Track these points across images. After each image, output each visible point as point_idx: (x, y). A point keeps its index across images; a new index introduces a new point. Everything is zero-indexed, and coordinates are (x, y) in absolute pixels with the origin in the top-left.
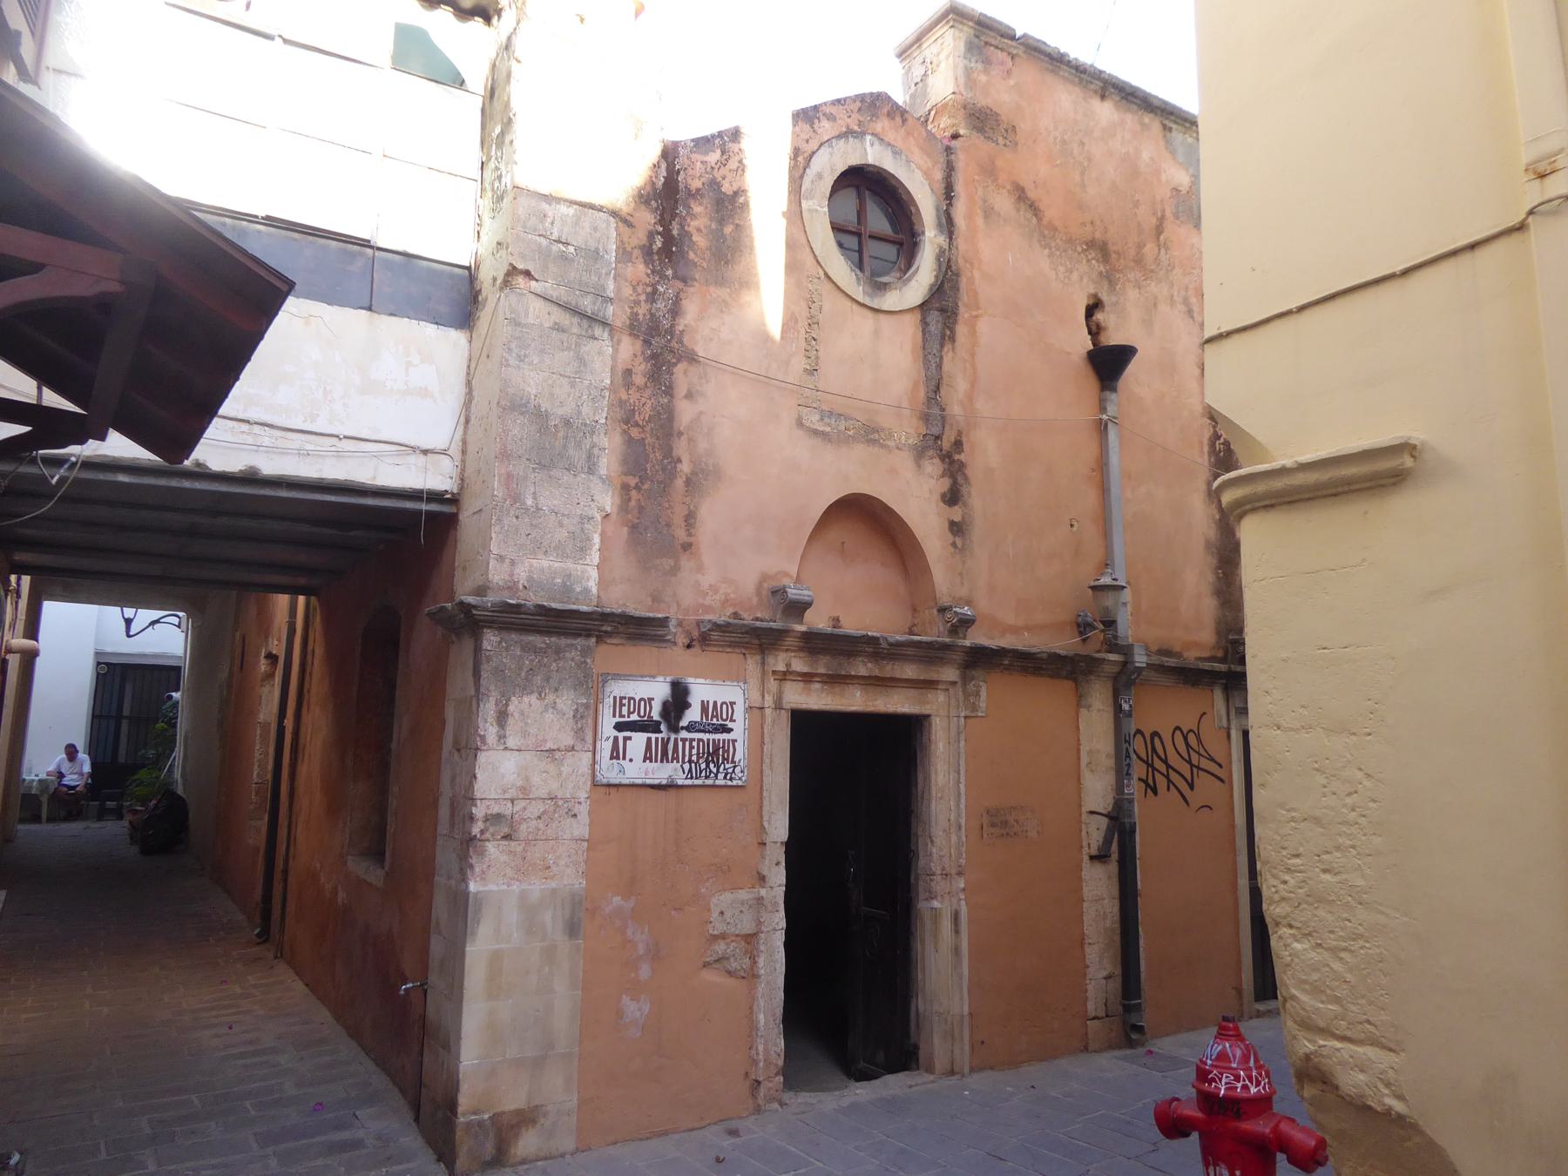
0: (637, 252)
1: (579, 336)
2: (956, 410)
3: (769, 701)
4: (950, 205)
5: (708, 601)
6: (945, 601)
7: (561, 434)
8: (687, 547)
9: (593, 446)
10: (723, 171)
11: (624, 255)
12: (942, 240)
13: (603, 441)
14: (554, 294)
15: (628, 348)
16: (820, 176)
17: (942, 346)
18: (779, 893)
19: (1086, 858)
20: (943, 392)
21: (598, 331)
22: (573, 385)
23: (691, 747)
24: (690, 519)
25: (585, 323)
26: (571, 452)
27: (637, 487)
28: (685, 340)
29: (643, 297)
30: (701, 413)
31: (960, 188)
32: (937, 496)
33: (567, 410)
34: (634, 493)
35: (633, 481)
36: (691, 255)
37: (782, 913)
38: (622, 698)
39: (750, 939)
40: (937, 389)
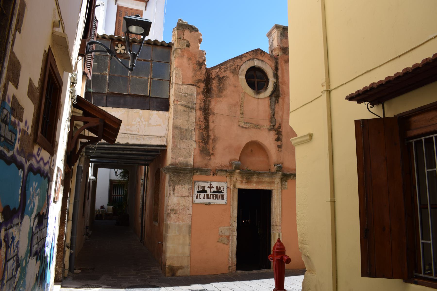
0: (201, 93)
2: (278, 120)
3: (232, 186)
4: (277, 71)
5: (218, 165)
8: (212, 154)
9: (192, 134)
10: (220, 73)
11: (198, 94)
13: (194, 133)
15: (199, 113)
16: (243, 70)
17: (275, 104)
20: (275, 114)
21: (192, 110)
22: (187, 122)
24: (213, 148)
27: (202, 142)
28: (212, 110)
31: (279, 67)
32: (274, 139)
33: (186, 128)
35: (201, 141)
36: (213, 92)
39: (228, 237)
40: (274, 115)
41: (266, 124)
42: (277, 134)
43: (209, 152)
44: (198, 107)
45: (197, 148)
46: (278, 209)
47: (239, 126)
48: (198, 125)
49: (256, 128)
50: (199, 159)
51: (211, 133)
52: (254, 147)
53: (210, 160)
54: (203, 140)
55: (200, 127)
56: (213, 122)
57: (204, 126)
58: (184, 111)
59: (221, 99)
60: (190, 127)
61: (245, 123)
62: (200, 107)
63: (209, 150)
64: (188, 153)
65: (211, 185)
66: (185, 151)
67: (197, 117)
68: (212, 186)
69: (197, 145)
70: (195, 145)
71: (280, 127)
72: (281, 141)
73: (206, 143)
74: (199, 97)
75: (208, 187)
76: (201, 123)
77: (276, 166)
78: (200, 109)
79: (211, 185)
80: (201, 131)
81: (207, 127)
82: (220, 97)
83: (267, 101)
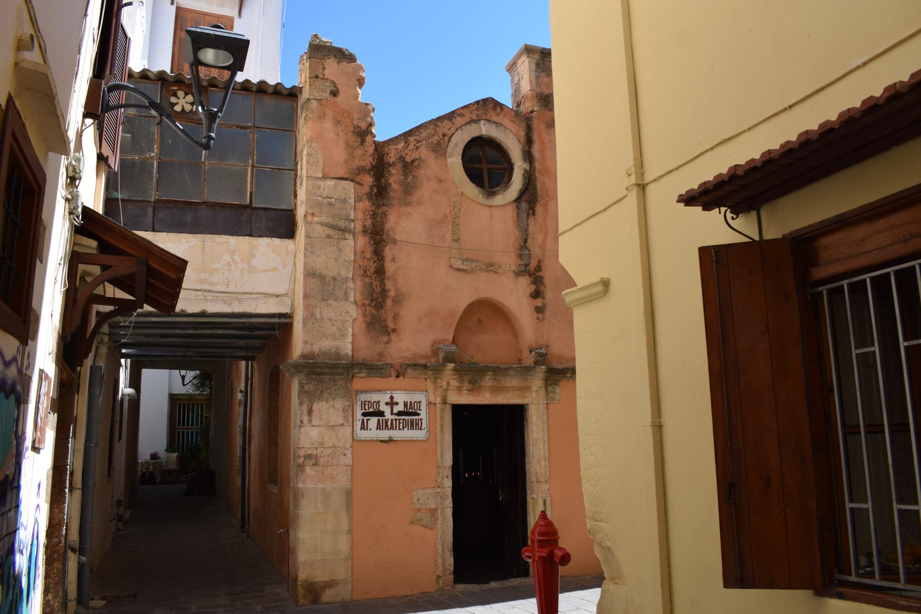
0: (364, 197)
3: (438, 400)
8: (394, 330)
9: (347, 288)
10: (406, 151)
11: (358, 199)
12: (526, 166)
15: (362, 241)
16: (456, 145)
17: (528, 218)
21: (347, 235)
22: (336, 261)
24: (396, 317)
25: (341, 233)
27: (369, 305)
28: (390, 233)
31: (535, 137)
32: (527, 295)
33: (334, 273)
34: (368, 308)
35: (367, 302)
39: (433, 512)
40: (526, 241)
41: (510, 262)
42: (534, 283)
43: (387, 327)
44: (359, 228)
45: (360, 318)
47: (451, 267)
48: (360, 267)
49: (488, 271)
50: (364, 342)
51: (389, 285)
52: (485, 312)
53: (388, 342)
54: (372, 301)
55: (365, 271)
56: (393, 260)
57: (373, 269)
58: (329, 236)
59: (409, 209)
60: (343, 273)
62: (364, 227)
63: (385, 321)
64: (339, 329)
65: (392, 398)
66: (333, 325)
67: (358, 251)
68: (395, 400)
69: (360, 312)
70: (354, 312)
71: (539, 268)
72: (544, 298)
75: (387, 404)
76: (366, 263)
79: (392, 398)
80: (367, 280)
81: (380, 271)
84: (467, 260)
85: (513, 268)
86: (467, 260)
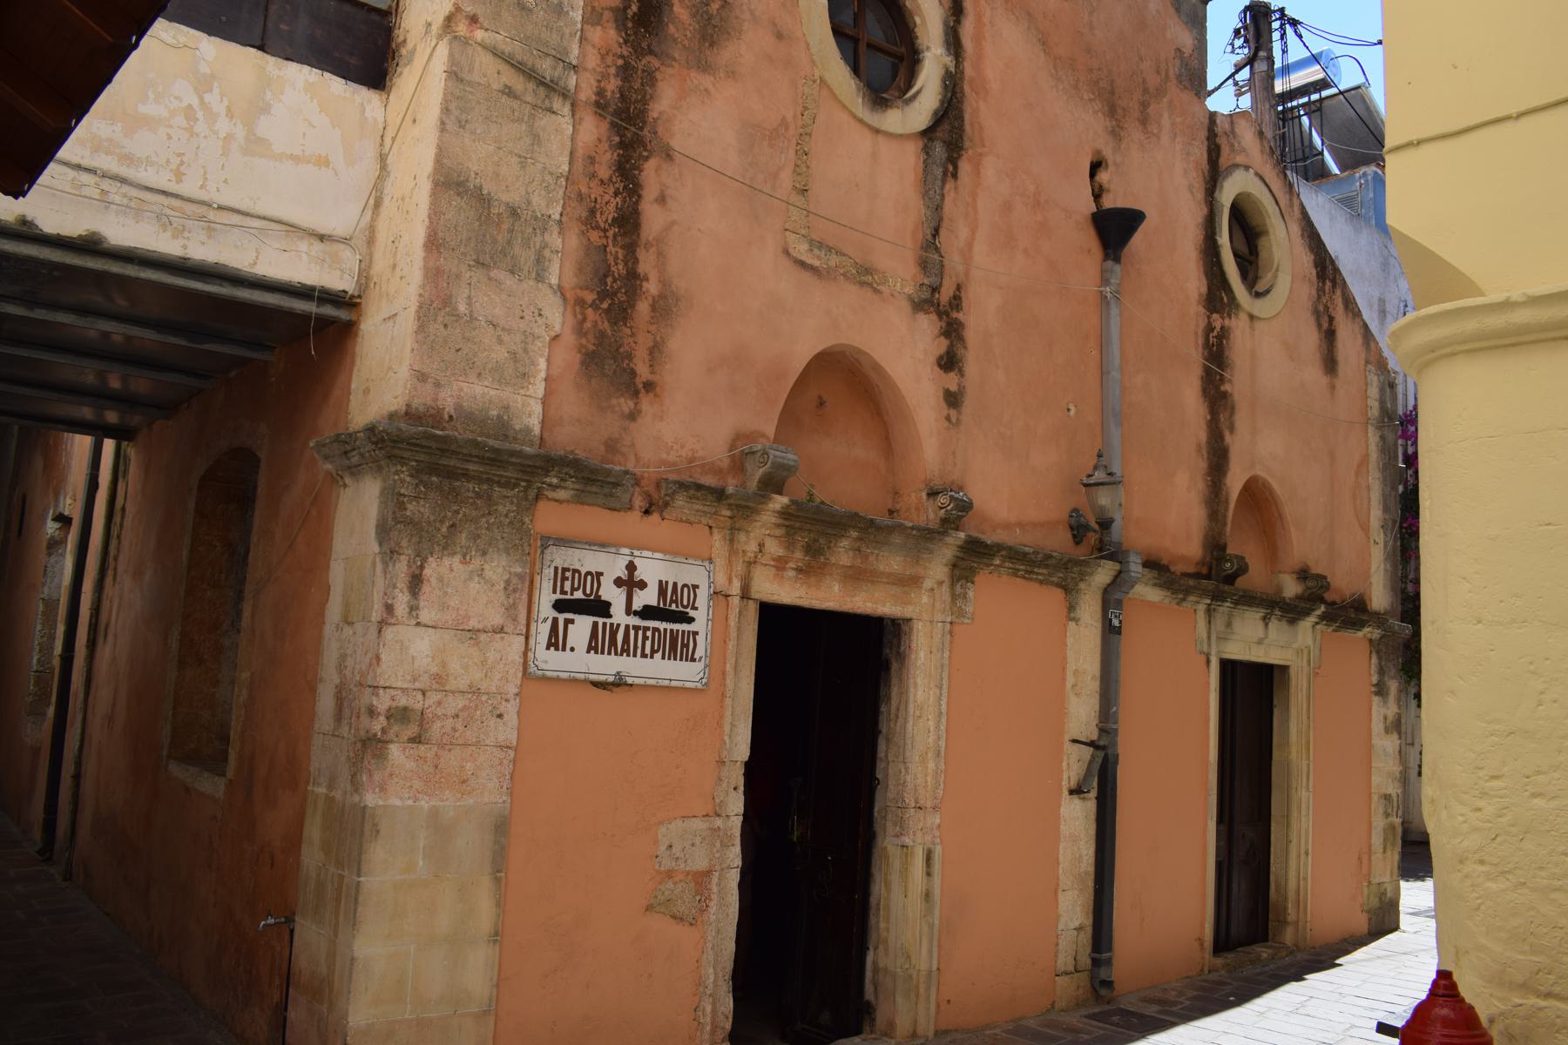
0: (607, 15)
1: (534, 106)
2: (954, 261)
3: (736, 588)
4: (958, 22)
6: (937, 483)
7: (505, 226)
8: (649, 386)
9: (545, 246)
13: (555, 240)
14: (508, 48)
15: (592, 130)
17: (944, 182)
18: (737, 822)
19: (1066, 793)
20: (942, 232)
21: (557, 104)
22: (523, 165)
23: (645, 638)
24: (656, 351)
25: (542, 91)
26: (517, 250)
28: (660, 130)
29: (612, 71)
30: (674, 223)
32: (932, 359)
33: (514, 197)
36: (672, 29)
37: (737, 849)
38: (565, 570)
40: (936, 232)
41: (902, 274)
43: (633, 373)
44: (587, 94)
45: (569, 338)
46: (931, 724)
47: (786, 252)
48: (580, 197)
49: (862, 284)
50: (573, 404)
53: (633, 416)
54: (603, 295)
57: (610, 213)
58: (509, 92)
59: (706, 81)
61: (811, 242)
62: (600, 93)
65: (631, 567)
66: (500, 341)
67: (580, 153)
70: (556, 317)
71: (956, 302)
72: (961, 373)
73: (620, 313)
74: (596, 34)
75: (618, 582)
76: (596, 191)
77: (942, 499)
78: (597, 104)
79: (631, 567)
80: (595, 236)
81: (628, 222)
82: (706, 68)
83: (910, 155)
84: (820, 245)
85: (909, 290)
86: (820, 245)
